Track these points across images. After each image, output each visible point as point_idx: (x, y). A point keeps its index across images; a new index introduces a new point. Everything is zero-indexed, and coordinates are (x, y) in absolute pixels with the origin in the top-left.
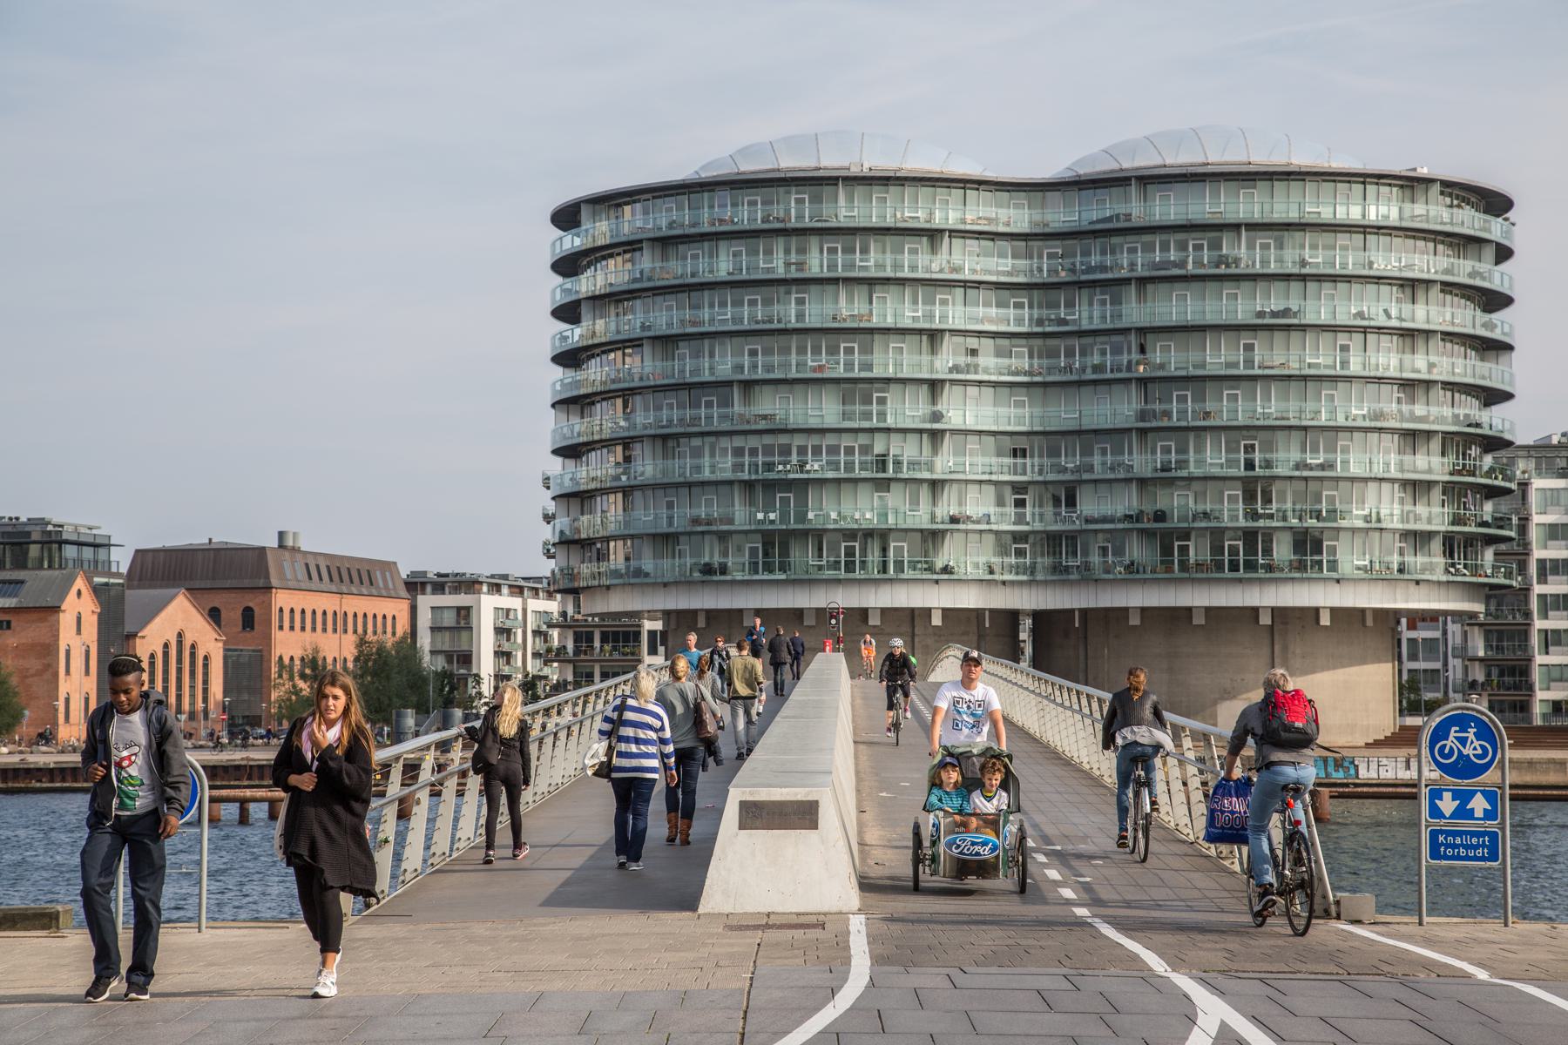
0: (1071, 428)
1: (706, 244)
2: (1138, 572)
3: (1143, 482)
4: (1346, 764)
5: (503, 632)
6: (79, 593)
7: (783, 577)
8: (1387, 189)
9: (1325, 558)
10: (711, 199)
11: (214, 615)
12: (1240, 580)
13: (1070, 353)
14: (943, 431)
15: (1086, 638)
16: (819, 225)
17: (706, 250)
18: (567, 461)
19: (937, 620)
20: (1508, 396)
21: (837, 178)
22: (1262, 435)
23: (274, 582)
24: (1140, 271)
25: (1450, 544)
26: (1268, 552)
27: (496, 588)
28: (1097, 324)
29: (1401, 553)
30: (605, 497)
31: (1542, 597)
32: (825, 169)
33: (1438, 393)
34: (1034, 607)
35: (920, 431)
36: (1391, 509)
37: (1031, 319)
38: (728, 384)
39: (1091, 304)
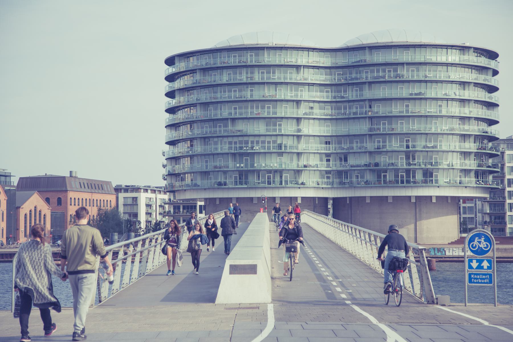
0: (346, 134)
1: (219, 71)
2: (369, 184)
3: (371, 153)
4: (442, 250)
5: (149, 206)
7: (246, 186)
8: (455, 50)
10: (220, 55)
11: (47, 200)
12: (405, 187)
13: (345, 108)
14: (301, 135)
15: (351, 207)
16: (258, 64)
17: (219, 73)
18: (170, 146)
20: (496, 122)
21: (264, 48)
22: (411, 136)
23: (68, 189)
24: (369, 80)
25: (477, 174)
26: (414, 177)
27: (146, 191)
28: (354, 98)
29: (460, 177)
30: (184, 159)
31: (509, 192)
33: (473, 121)
34: (333, 196)
35: (293, 135)
36: (457, 162)
37: (331, 96)
38: (227, 119)
39: (352, 91)
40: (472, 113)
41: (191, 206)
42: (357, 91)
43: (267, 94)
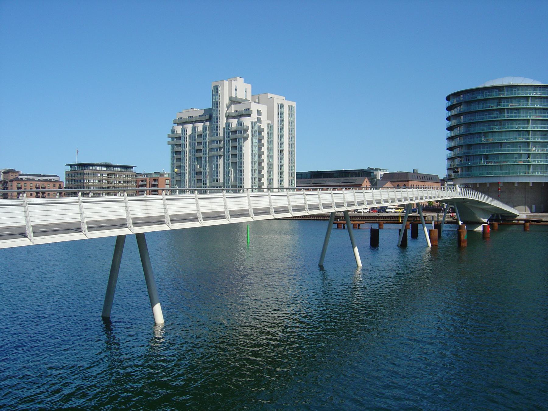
6: (366, 181)
19: (531, 185)
38: (480, 133)
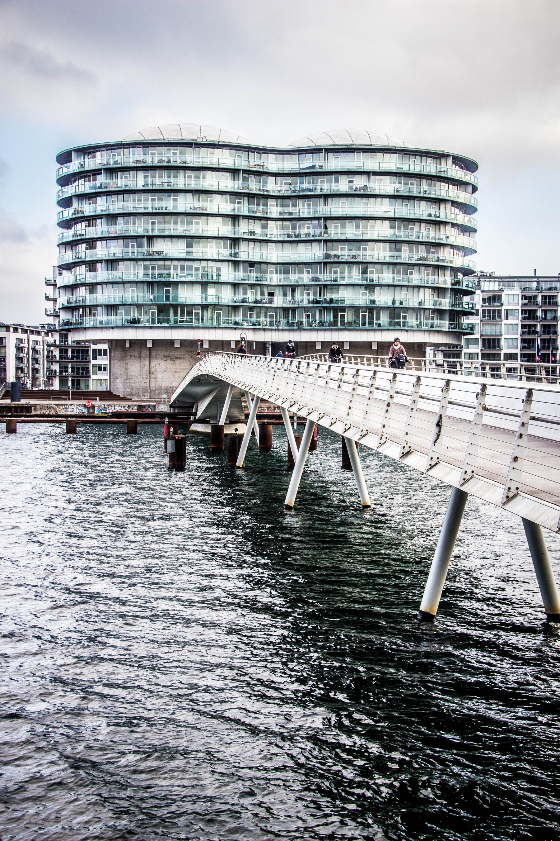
1: (131, 172)
5: (19, 349)
7: (168, 325)
9: (402, 320)
10: (133, 152)
14: (239, 261)
16: (184, 165)
21: (192, 144)
26: (378, 318)
27: (16, 330)
28: (306, 216)
32: (185, 140)
38: (142, 237)
39: (303, 206)
40: (448, 240)
41: (83, 350)
42: (309, 205)
43: (196, 206)
